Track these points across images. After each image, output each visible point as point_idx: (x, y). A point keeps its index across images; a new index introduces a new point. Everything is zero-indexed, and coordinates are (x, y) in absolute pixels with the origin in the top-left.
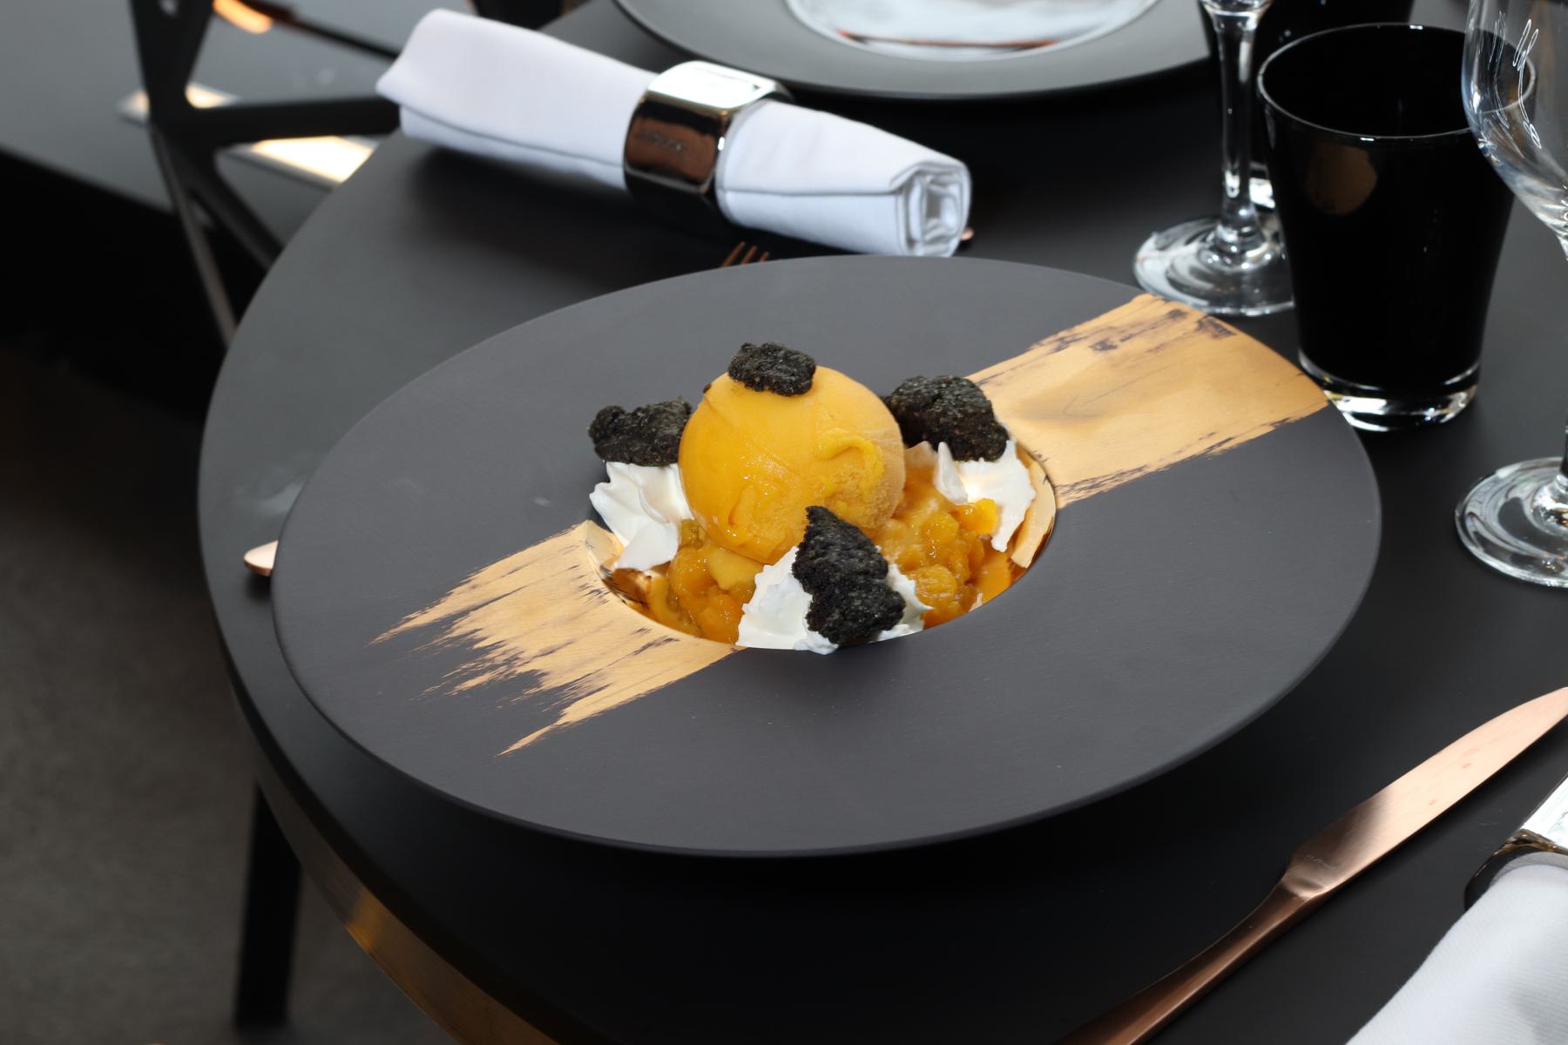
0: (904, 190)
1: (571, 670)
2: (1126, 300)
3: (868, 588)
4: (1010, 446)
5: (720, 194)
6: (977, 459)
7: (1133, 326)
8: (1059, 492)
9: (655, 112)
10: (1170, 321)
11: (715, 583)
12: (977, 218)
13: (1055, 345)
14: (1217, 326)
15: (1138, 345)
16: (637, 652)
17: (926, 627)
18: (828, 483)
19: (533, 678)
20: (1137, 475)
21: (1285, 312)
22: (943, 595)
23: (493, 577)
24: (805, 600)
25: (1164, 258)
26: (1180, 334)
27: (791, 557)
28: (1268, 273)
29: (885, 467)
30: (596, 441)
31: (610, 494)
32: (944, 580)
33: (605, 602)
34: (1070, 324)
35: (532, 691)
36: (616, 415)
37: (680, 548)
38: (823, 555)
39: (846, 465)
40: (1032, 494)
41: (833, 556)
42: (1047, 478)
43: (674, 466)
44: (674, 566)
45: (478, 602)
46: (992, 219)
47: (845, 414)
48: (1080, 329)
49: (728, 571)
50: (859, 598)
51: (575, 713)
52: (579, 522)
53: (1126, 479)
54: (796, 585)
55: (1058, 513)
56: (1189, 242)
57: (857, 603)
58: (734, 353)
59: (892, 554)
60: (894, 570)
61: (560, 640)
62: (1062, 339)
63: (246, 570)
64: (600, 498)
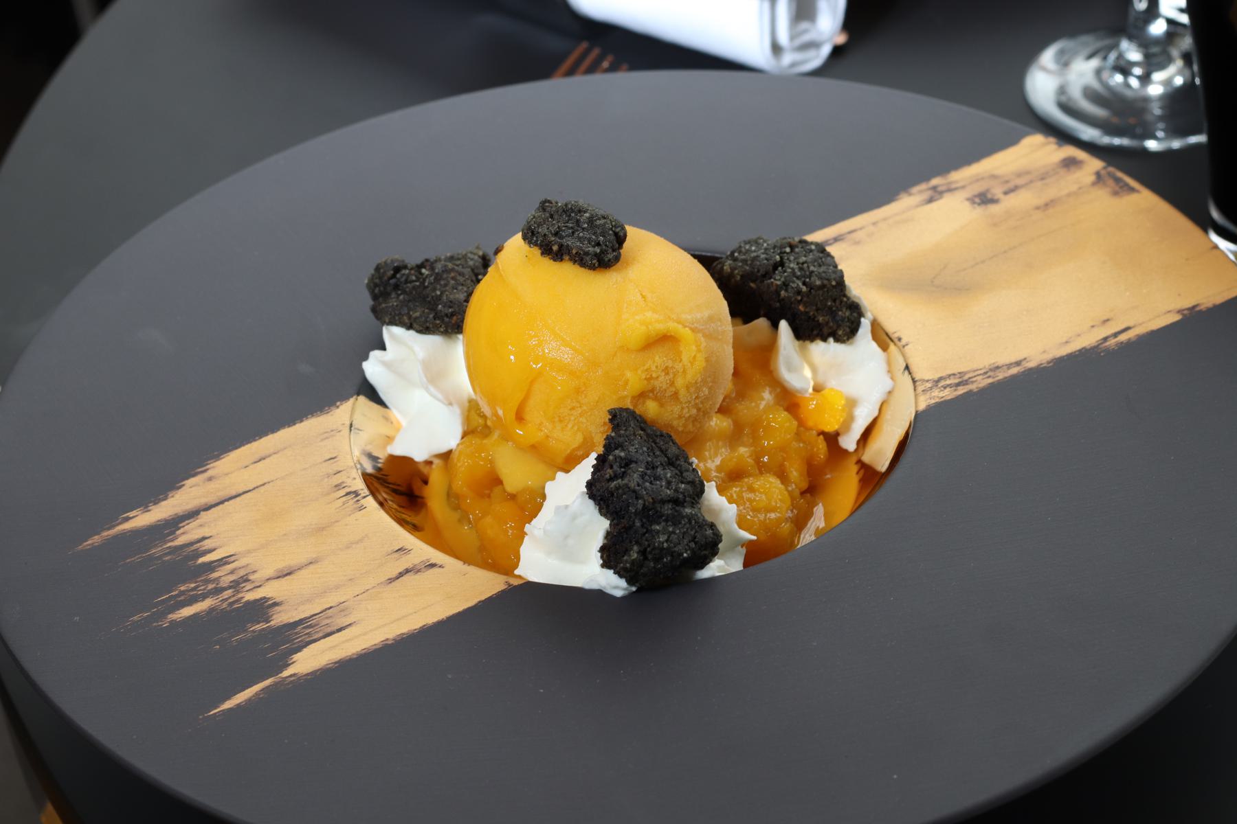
1: (309, 601)
2: (1011, 141)
3: (675, 519)
4: (865, 323)
6: (824, 339)
7: (1019, 175)
8: (920, 389)
10: (1062, 171)
11: (498, 481)
12: (853, 20)
13: (929, 193)
14: (1117, 180)
15: (1023, 200)
16: (391, 580)
17: (746, 565)
18: (634, 380)
19: (262, 608)
20: (1014, 371)
21: (1197, 146)
22: (773, 515)
23: (232, 468)
24: (598, 527)
25: (1057, 76)
26: (1074, 188)
27: (585, 470)
28: (1175, 98)
29: (707, 360)
30: (375, 297)
31: (386, 364)
32: (773, 494)
33: (362, 508)
34: (944, 170)
35: (258, 627)
36: (397, 270)
37: (465, 435)
38: (623, 476)
39: (658, 359)
40: (887, 384)
41: (633, 479)
42: (907, 368)
43: (460, 336)
44: (455, 456)
45: (211, 499)
47: (664, 287)
48: (960, 176)
49: (516, 472)
50: (664, 531)
51: (306, 661)
52: (345, 398)
53: (1001, 376)
54: (590, 508)
55: (917, 415)
56: (1090, 57)
57: (662, 538)
58: (530, 211)
59: (709, 462)
60: (712, 495)
61: (303, 559)
62: (934, 188)
64: (374, 368)
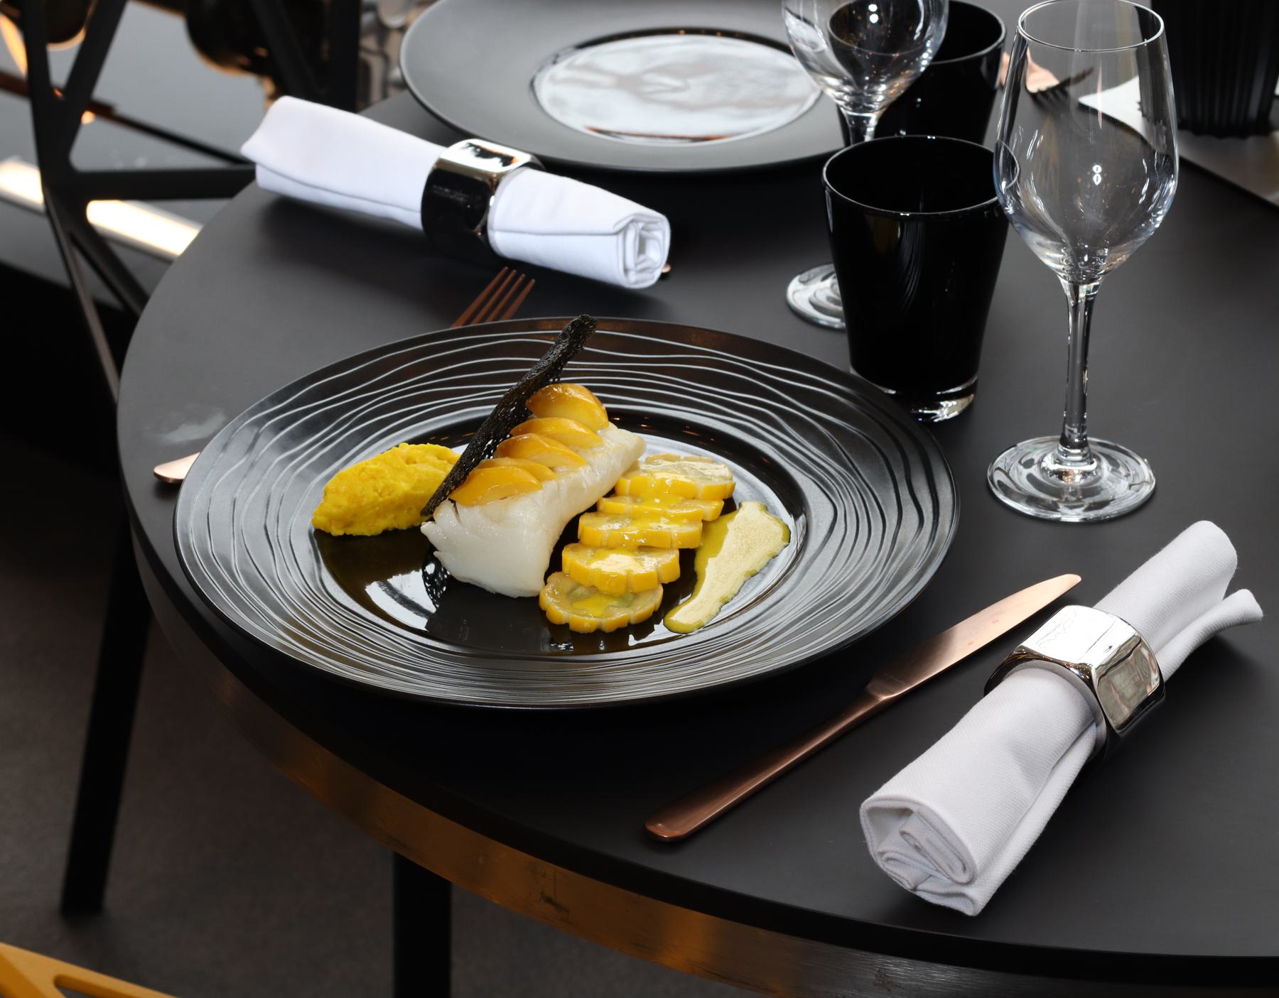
0: (624, 230)
5: (490, 233)
9: (442, 177)
12: (675, 256)
46: (682, 251)
56: (824, 279)
63: (156, 479)
